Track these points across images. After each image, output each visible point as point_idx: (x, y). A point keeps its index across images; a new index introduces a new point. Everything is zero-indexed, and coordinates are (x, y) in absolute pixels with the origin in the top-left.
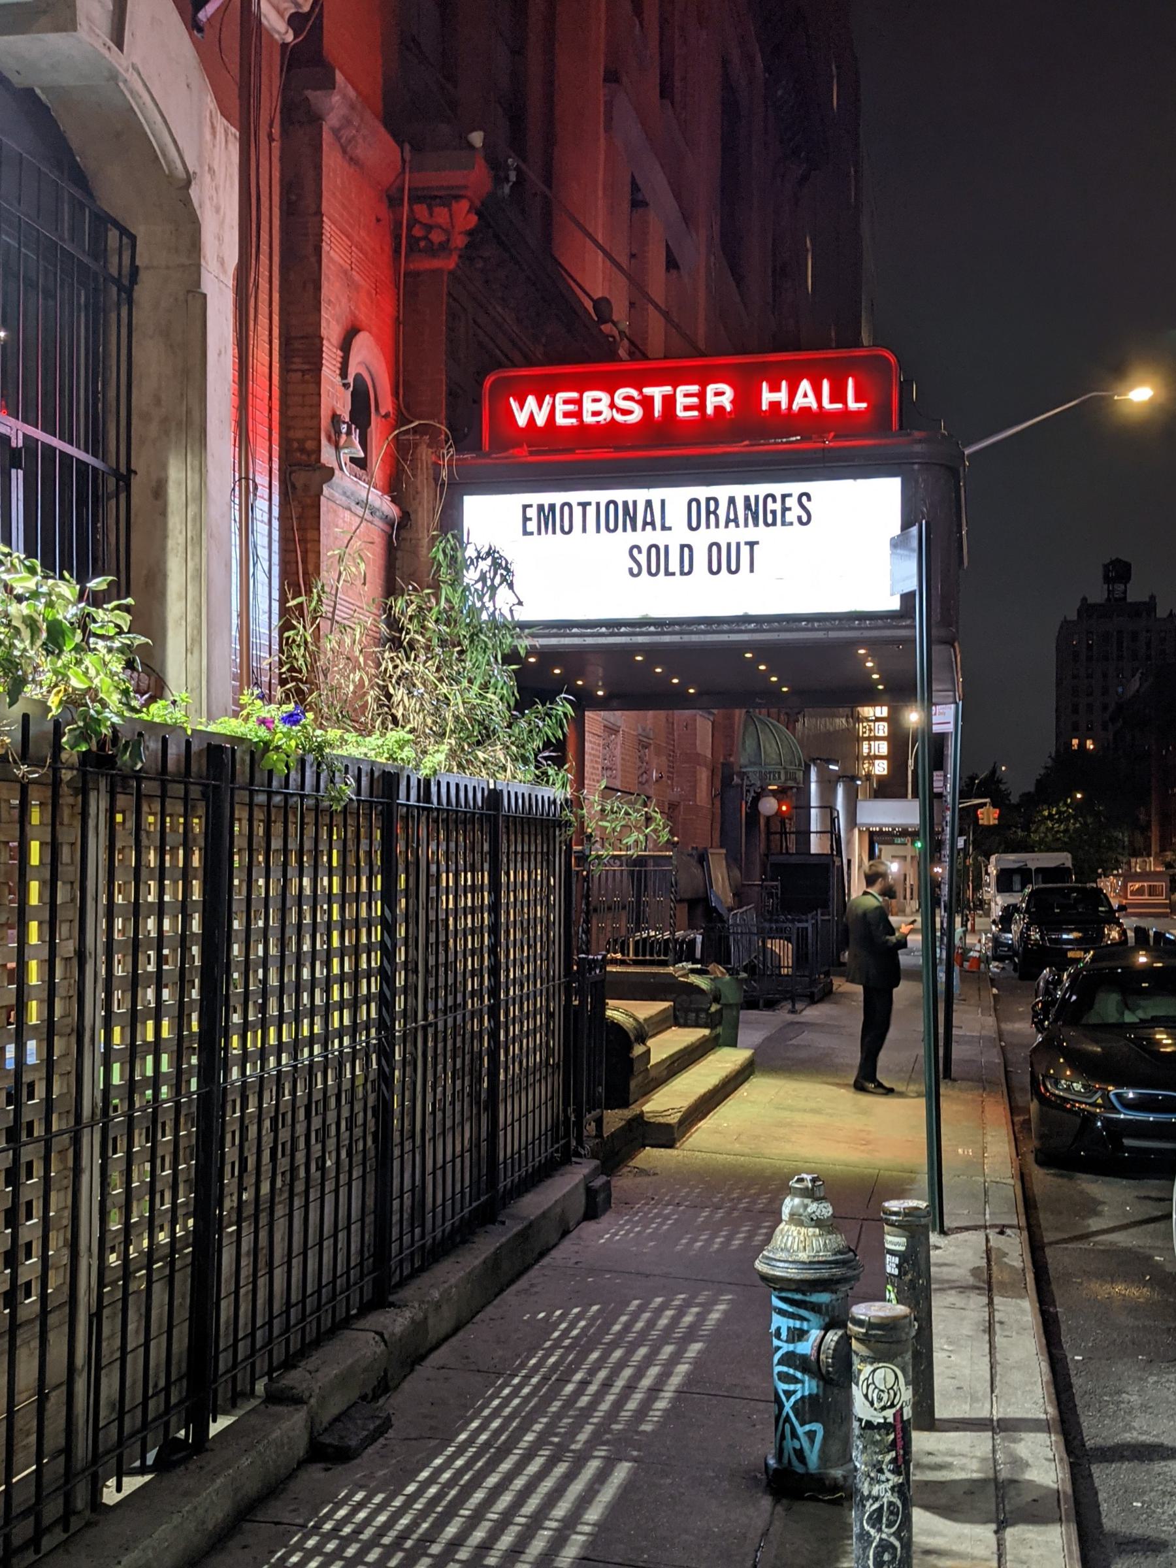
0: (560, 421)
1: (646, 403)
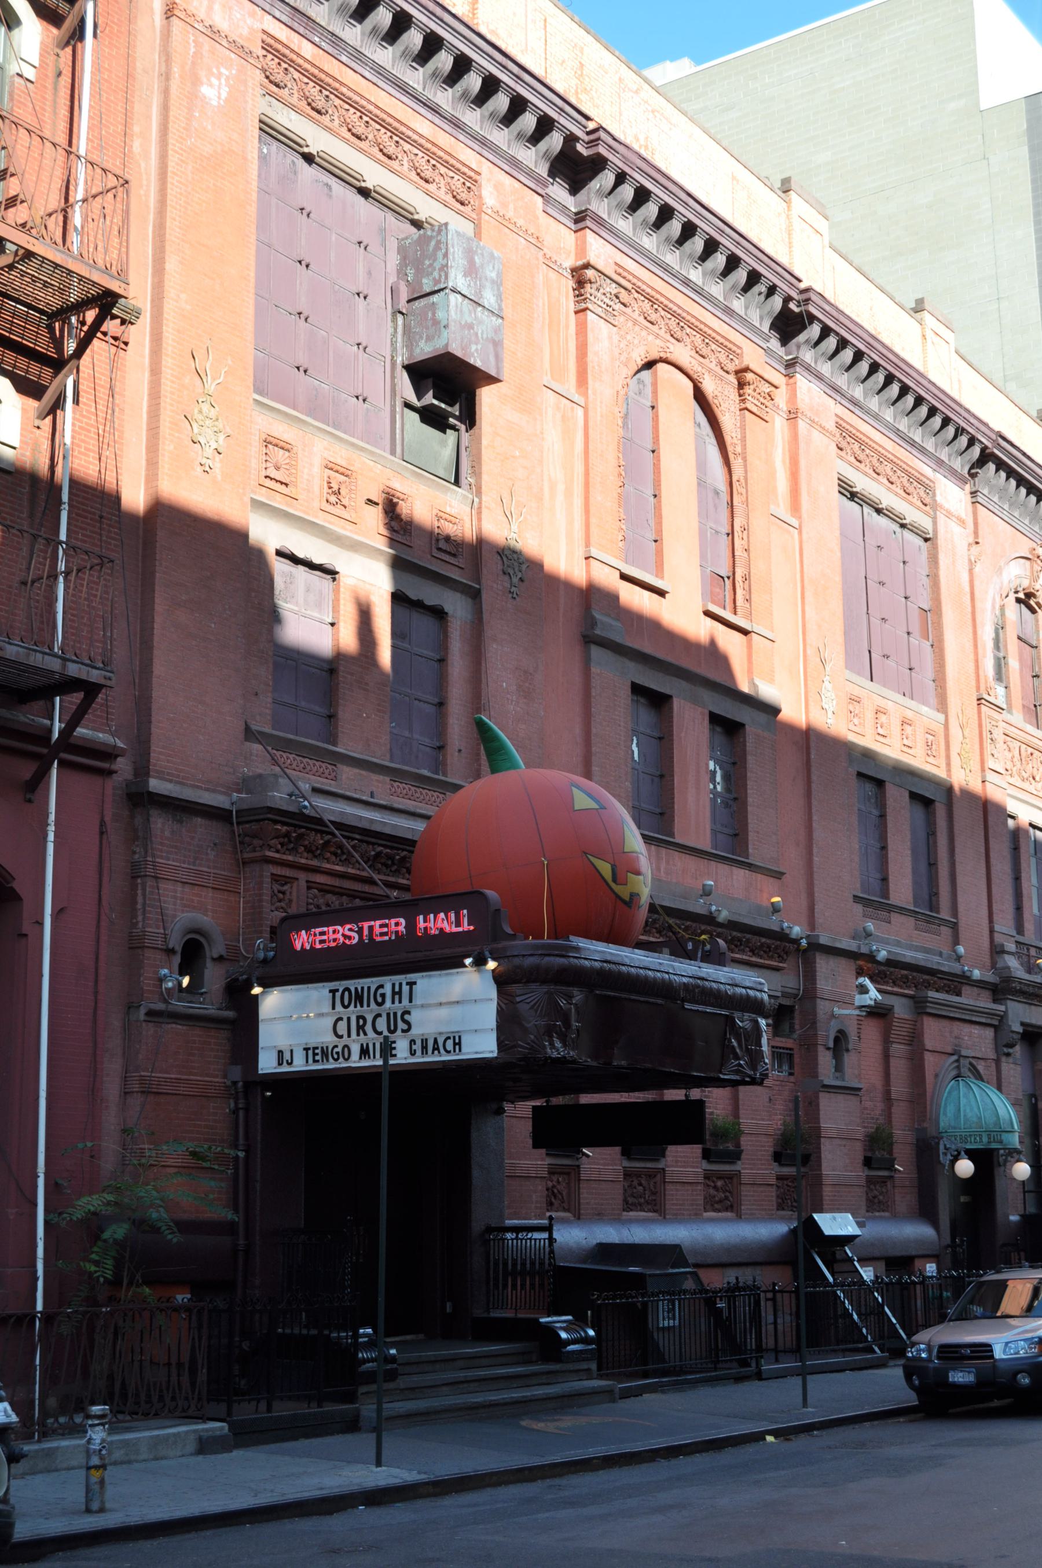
1: (360, 932)
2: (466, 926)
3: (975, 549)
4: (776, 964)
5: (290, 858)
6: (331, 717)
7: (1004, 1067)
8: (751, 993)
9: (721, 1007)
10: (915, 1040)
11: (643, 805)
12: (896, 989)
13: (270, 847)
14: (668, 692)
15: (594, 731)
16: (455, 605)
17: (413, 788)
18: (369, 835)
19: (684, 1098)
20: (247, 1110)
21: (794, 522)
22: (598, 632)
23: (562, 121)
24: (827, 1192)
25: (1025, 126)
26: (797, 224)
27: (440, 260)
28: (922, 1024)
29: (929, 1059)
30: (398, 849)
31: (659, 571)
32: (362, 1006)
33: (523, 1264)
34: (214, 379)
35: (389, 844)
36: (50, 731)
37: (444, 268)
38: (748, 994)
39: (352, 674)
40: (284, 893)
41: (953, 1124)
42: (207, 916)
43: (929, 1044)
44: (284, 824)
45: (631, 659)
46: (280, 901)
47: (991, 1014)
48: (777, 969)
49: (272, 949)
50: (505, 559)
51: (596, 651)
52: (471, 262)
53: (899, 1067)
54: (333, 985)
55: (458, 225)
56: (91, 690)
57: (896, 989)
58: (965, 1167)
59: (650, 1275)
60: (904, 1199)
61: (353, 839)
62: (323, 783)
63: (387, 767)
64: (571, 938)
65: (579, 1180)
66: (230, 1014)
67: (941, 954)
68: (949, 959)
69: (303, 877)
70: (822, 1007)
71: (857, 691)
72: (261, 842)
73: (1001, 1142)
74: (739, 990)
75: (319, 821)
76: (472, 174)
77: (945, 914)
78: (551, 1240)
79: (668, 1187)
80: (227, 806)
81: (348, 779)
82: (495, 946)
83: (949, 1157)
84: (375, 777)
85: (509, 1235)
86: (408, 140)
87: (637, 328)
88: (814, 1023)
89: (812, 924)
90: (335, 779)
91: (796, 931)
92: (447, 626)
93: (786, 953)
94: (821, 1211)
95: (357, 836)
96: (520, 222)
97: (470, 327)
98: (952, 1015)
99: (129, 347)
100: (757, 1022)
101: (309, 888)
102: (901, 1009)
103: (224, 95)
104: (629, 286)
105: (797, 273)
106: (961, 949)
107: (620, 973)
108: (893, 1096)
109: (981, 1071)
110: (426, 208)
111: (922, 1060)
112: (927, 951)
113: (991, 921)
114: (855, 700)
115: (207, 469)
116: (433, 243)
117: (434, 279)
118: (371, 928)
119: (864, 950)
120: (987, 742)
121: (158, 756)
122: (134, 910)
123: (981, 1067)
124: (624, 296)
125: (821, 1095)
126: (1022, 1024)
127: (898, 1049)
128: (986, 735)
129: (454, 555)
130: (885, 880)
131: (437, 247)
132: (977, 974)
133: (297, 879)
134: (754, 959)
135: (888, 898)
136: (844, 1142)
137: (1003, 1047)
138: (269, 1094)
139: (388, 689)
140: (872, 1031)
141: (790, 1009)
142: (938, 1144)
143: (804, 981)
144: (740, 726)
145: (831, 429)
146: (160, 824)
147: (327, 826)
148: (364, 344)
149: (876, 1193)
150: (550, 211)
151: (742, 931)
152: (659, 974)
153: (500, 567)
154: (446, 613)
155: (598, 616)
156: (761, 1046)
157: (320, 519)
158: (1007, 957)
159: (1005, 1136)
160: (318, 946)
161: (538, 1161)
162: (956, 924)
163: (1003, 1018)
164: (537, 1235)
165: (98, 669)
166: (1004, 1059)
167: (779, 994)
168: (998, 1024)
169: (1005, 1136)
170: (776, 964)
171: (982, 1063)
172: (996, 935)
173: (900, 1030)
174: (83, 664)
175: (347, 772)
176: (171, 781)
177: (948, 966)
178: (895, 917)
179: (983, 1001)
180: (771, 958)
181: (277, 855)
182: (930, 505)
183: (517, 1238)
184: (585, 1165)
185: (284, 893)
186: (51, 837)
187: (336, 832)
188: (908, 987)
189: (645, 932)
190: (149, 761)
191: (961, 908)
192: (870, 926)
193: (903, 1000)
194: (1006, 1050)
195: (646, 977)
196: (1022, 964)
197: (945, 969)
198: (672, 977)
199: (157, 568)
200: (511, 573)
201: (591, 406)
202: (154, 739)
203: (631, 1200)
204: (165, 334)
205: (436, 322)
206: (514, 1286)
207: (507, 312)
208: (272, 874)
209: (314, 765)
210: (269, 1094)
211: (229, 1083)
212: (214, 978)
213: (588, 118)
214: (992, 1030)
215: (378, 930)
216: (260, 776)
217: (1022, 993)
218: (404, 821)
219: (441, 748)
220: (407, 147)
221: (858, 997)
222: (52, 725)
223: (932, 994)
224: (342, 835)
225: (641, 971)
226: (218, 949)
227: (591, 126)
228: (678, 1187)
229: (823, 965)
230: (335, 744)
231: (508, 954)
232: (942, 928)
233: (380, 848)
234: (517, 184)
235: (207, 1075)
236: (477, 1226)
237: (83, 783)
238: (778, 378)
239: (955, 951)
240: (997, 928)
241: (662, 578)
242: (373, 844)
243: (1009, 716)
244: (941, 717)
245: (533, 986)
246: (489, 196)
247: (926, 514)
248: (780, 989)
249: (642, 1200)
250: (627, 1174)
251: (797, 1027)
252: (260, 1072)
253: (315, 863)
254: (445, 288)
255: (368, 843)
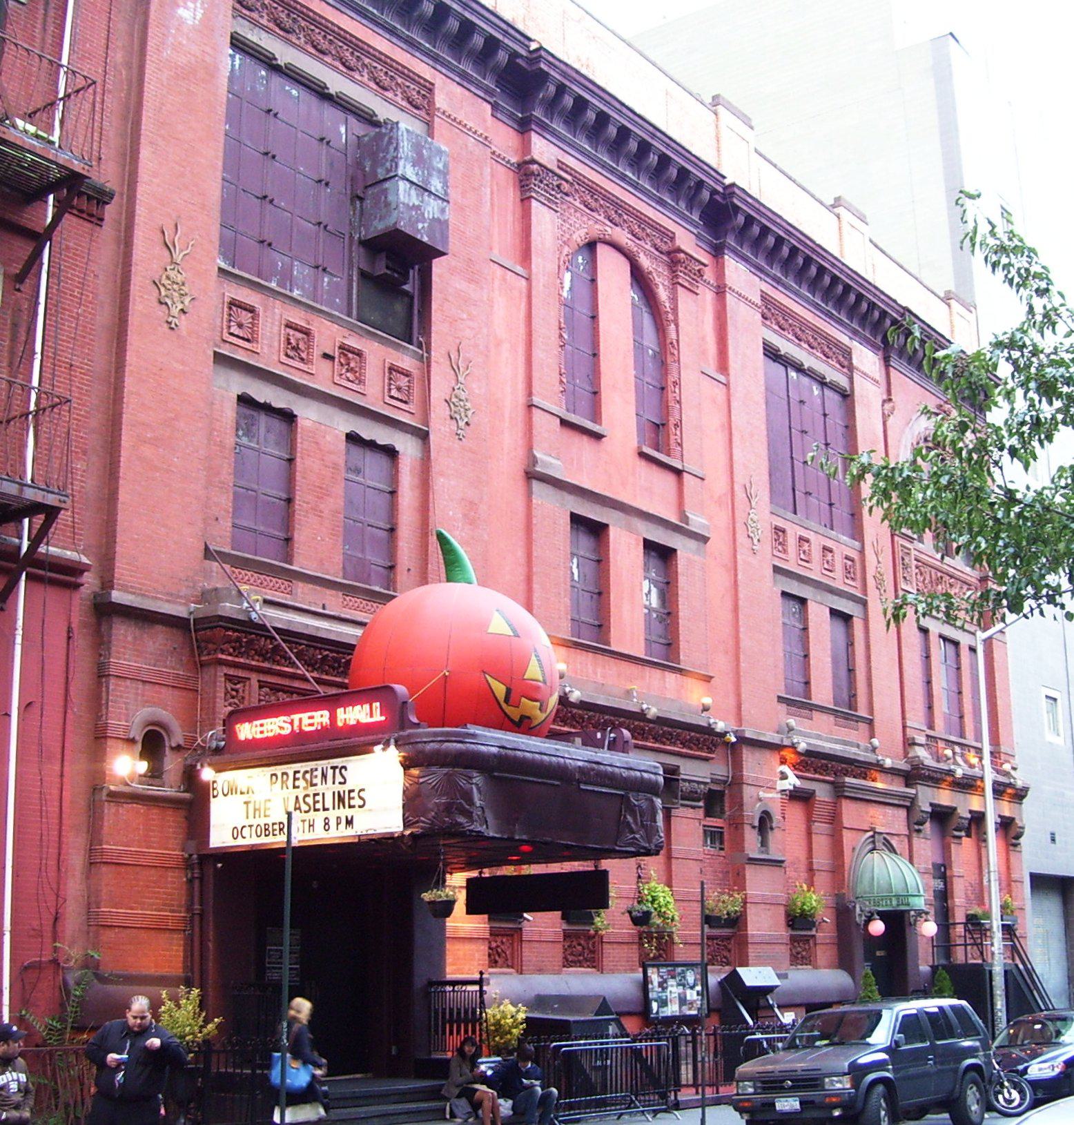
1: (292, 723)
2: (377, 717)
3: (887, 406)
4: (704, 754)
5: (242, 660)
6: (288, 540)
7: (915, 841)
8: (646, 775)
9: (616, 788)
10: (835, 820)
11: (583, 618)
12: (817, 776)
13: (223, 652)
14: (605, 521)
15: (535, 554)
16: (407, 446)
17: (364, 602)
18: (315, 641)
19: (593, 869)
20: (201, 879)
21: (722, 378)
22: (538, 469)
23: (506, 41)
24: (752, 952)
26: (724, 133)
27: (392, 153)
28: (841, 806)
29: (847, 836)
30: (344, 653)
31: (596, 416)
32: (339, 792)
33: (459, 1013)
34: (181, 251)
35: (231, 626)
36: (19, 548)
37: (395, 160)
38: (642, 777)
39: (308, 503)
40: (237, 691)
41: (868, 889)
42: (166, 710)
43: (846, 823)
44: (234, 630)
45: (570, 493)
46: (233, 697)
47: (904, 797)
48: (706, 759)
49: (223, 740)
50: (452, 406)
51: (536, 485)
52: (420, 154)
53: (821, 843)
54: (273, 769)
55: (408, 125)
56: (52, 513)
57: (817, 776)
58: (878, 927)
59: (575, 1022)
60: (824, 953)
61: (301, 644)
62: (274, 596)
63: (340, 583)
64: (468, 726)
65: (522, 941)
66: (187, 795)
67: (858, 746)
68: (866, 750)
69: (254, 678)
70: (748, 792)
71: (780, 523)
72: (215, 646)
73: (908, 904)
74: (633, 773)
75: (263, 627)
77: (863, 712)
78: (482, 992)
79: (605, 946)
80: (185, 615)
81: (304, 595)
82: (401, 733)
83: (864, 918)
84: (328, 592)
85: (449, 988)
86: (368, 54)
87: (578, 215)
88: (741, 805)
89: (739, 719)
90: (290, 593)
91: (720, 726)
92: (398, 463)
93: (714, 745)
94: (745, 964)
95: (305, 642)
96: (470, 124)
97: (418, 208)
98: (868, 797)
99: (104, 223)
100: (652, 801)
101: (261, 687)
102: (822, 793)
103: (199, 16)
104: (569, 178)
105: (724, 173)
106: (875, 742)
107: (515, 757)
108: (815, 867)
109: (895, 845)
110: (383, 110)
111: (841, 836)
112: (845, 743)
113: (904, 718)
114: (779, 531)
115: (173, 326)
116: (386, 139)
118: (300, 720)
119: (786, 742)
120: (900, 567)
121: (122, 570)
122: (100, 705)
123: (894, 842)
124: (566, 187)
125: (747, 867)
126: (931, 804)
127: (820, 827)
128: (899, 561)
129: (405, 402)
130: (807, 683)
131: (390, 142)
132: (888, 763)
133: (249, 679)
134: (684, 750)
135: (810, 699)
136: (768, 907)
137: (914, 825)
138: (220, 865)
139: (342, 516)
140: (796, 813)
141: (721, 794)
142: (854, 907)
143: (733, 769)
144: (605, 527)
145: (756, 302)
146: (122, 632)
147: (269, 631)
148: (270, 198)
149: (799, 949)
150: (499, 116)
151: (672, 727)
152: (554, 759)
153: (448, 413)
154: (398, 452)
155: (538, 455)
156: (655, 822)
157: (278, 370)
158: (917, 748)
159: (911, 900)
161: (477, 925)
162: (872, 720)
163: (913, 800)
164: (470, 988)
165: (52, 493)
166: (915, 835)
167: (709, 781)
168: (910, 806)
169: (911, 900)
170: (704, 754)
171: (896, 837)
172: (908, 730)
173: (820, 811)
174: (39, 489)
175: (301, 587)
176: (134, 593)
177: (863, 755)
178: (815, 714)
179: (897, 787)
180: (701, 749)
181: (230, 658)
182: (848, 367)
183: (453, 991)
184: (526, 927)
185: (237, 691)
186: (19, 639)
187: (277, 637)
188: (828, 775)
189: (554, 721)
190: (113, 576)
191: (876, 706)
192: (792, 722)
193: (827, 787)
194: (916, 827)
195: (542, 761)
196: (931, 754)
197: (862, 759)
198: (568, 761)
199: (124, 410)
200: (458, 417)
201: (533, 277)
202: (118, 558)
203: (570, 958)
204: (138, 212)
205: (387, 204)
206: (451, 1033)
207: (453, 195)
208: (225, 675)
209: (240, 573)
210: (220, 865)
211: (186, 856)
212: (172, 764)
213: (530, 40)
215: (306, 721)
216: (216, 589)
217: (930, 778)
218: (351, 629)
219: (392, 568)
220: (367, 61)
221: (779, 782)
222: (21, 543)
223: (849, 780)
224: (283, 640)
225: (537, 756)
226: (178, 737)
227: (533, 46)
228: (615, 946)
229: (750, 758)
230: (291, 565)
231: (412, 741)
232: (860, 724)
233: (327, 653)
234: (467, 93)
235: (166, 849)
236: (419, 982)
237: (53, 596)
238: (704, 257)
239: (871, 743)
240: (909, 723)
241: (600, 424)
242: (297, 643)
243: (921, 545)
244: (857, 544)
245: (434, 769)
246: (440, 101)
247: (843, 374)
248: (709, 776)
249: (581, 958)
250: (567, 935)
251: (726, 809)
252: (212, 846)
253: (266, 665)
254: (396, 176)
255: (316, 648)
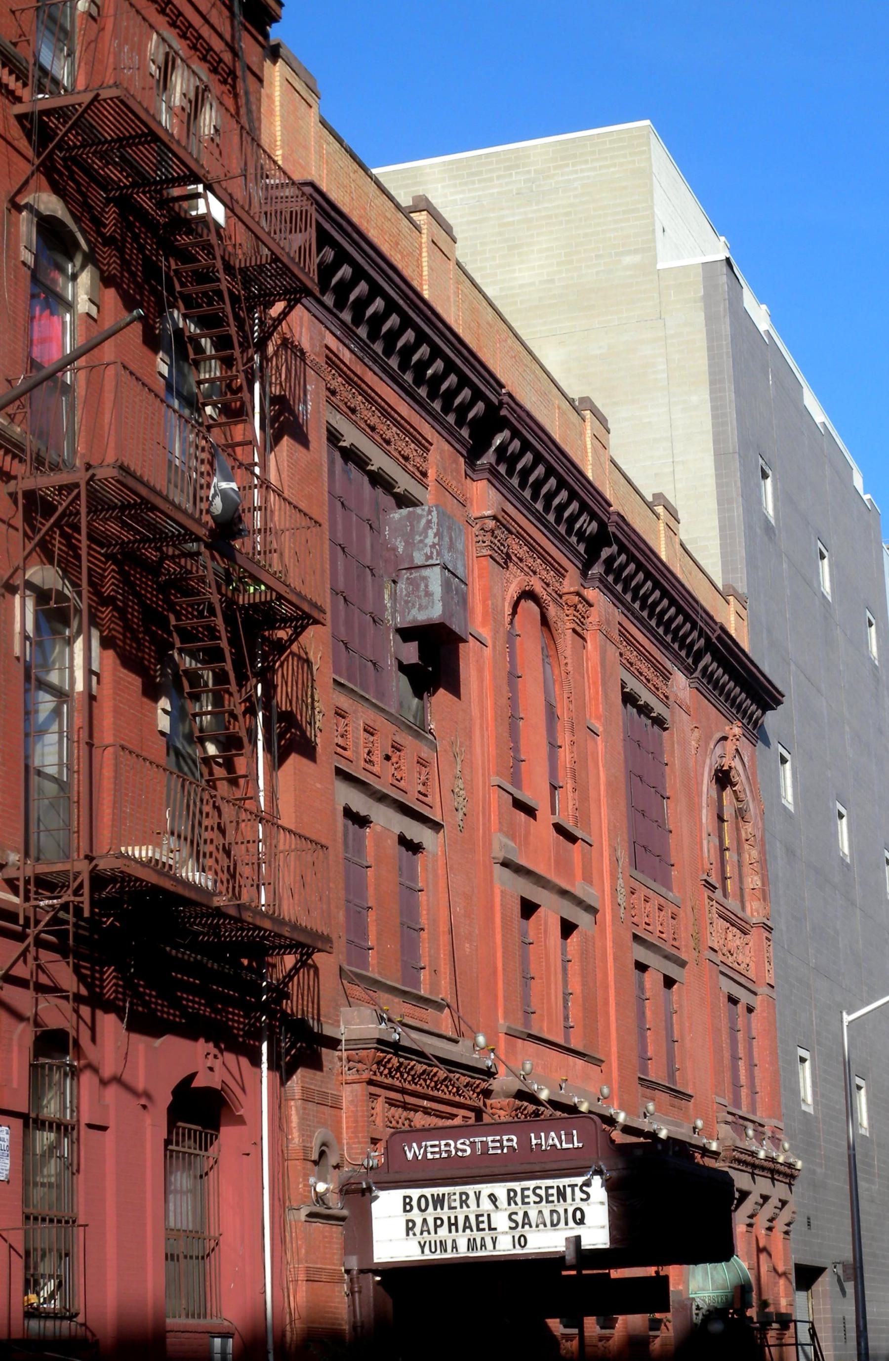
0: (430, 1156)
1: (473, 1145)
19: (654, 1274)
25: (702, 293)
76: (427, 444)
116: (423, 521)
117: (426, 554)
160: (430, 1156)
214: (19, 1123)
